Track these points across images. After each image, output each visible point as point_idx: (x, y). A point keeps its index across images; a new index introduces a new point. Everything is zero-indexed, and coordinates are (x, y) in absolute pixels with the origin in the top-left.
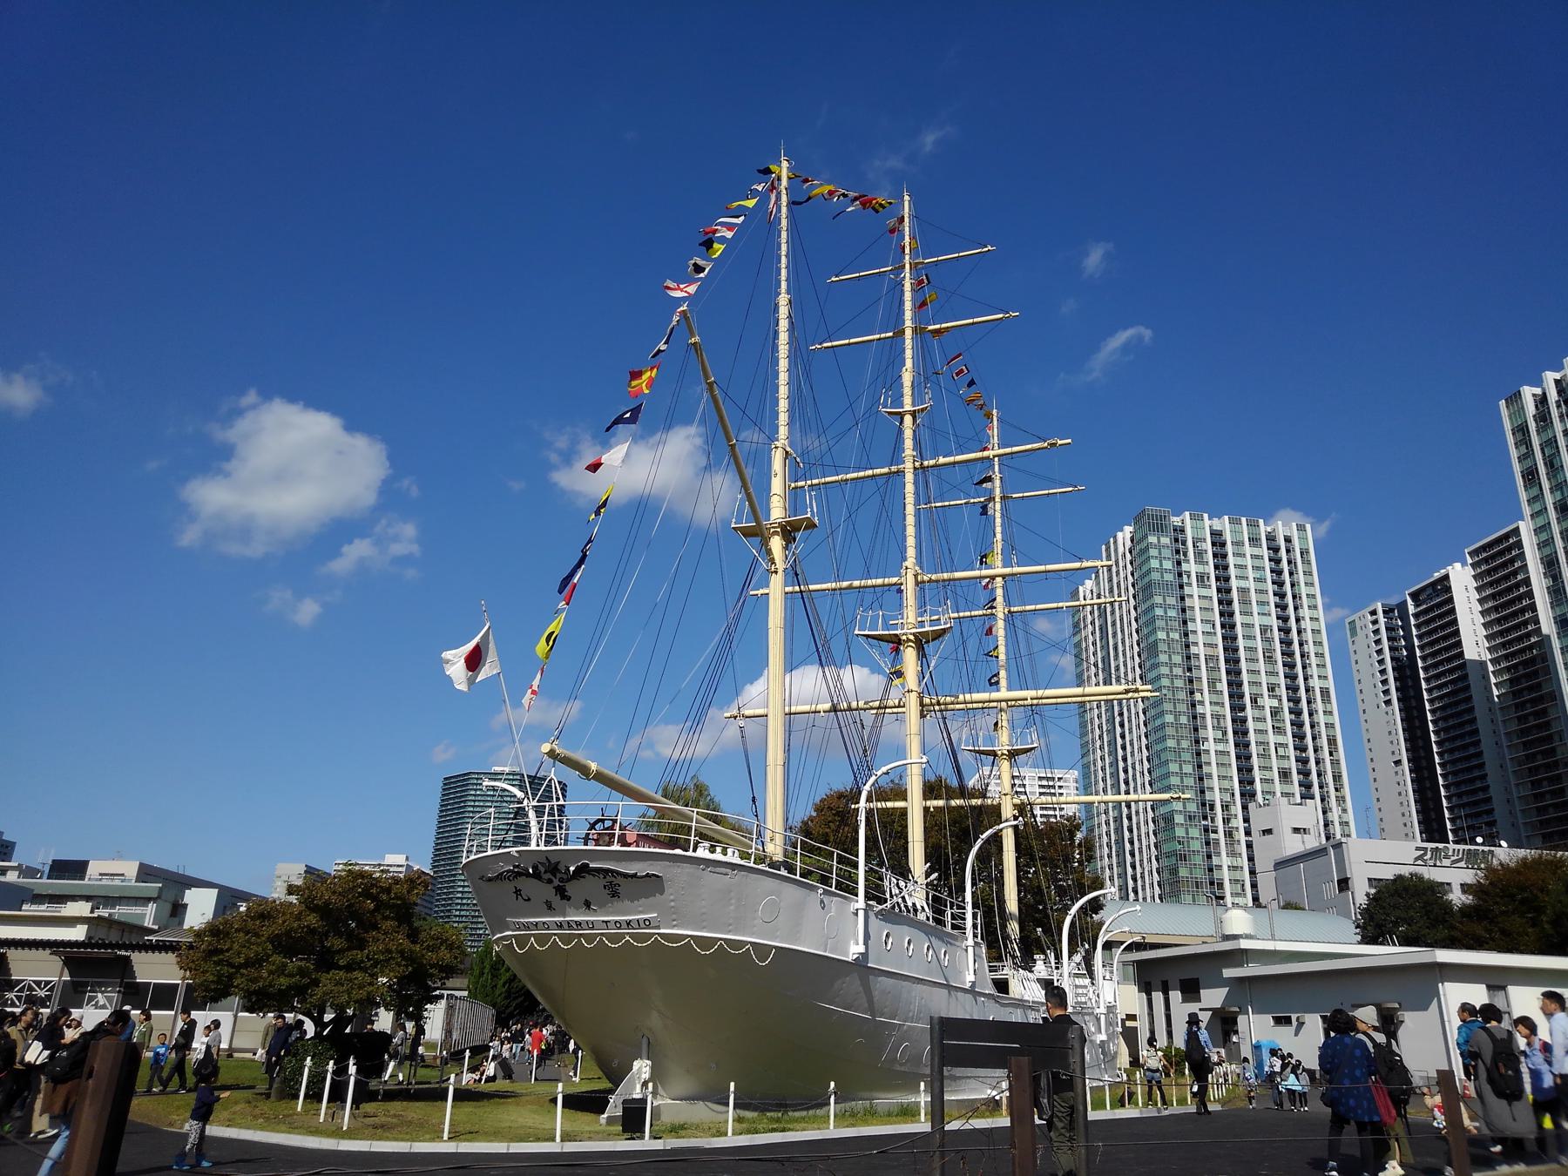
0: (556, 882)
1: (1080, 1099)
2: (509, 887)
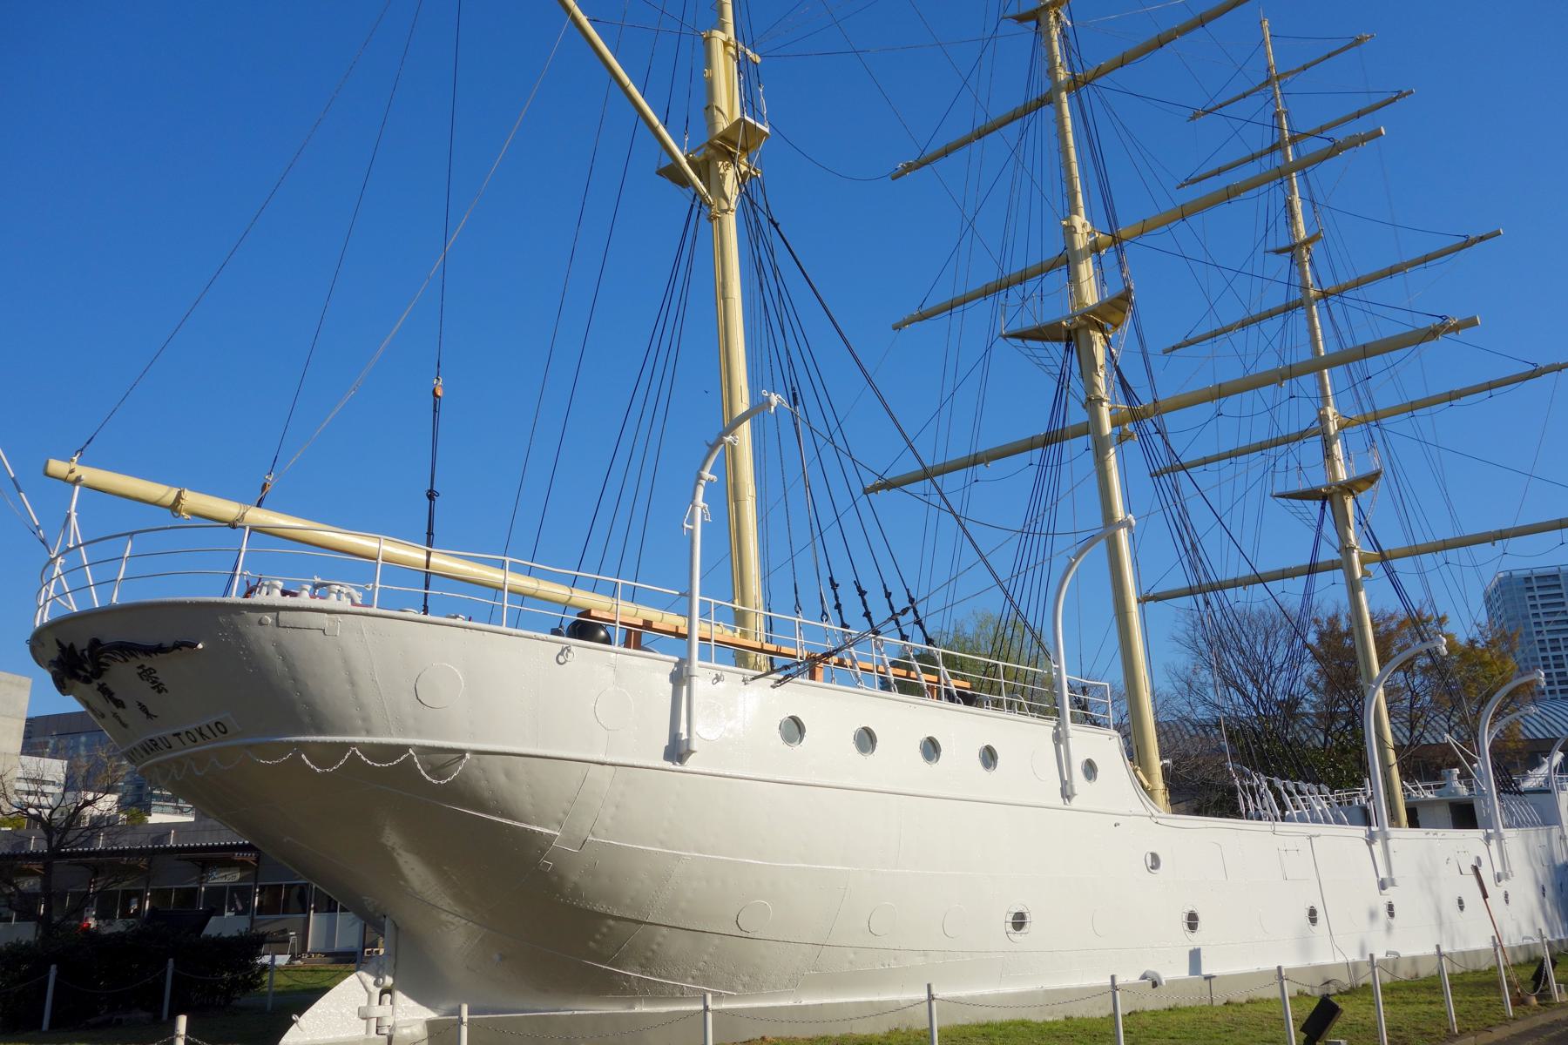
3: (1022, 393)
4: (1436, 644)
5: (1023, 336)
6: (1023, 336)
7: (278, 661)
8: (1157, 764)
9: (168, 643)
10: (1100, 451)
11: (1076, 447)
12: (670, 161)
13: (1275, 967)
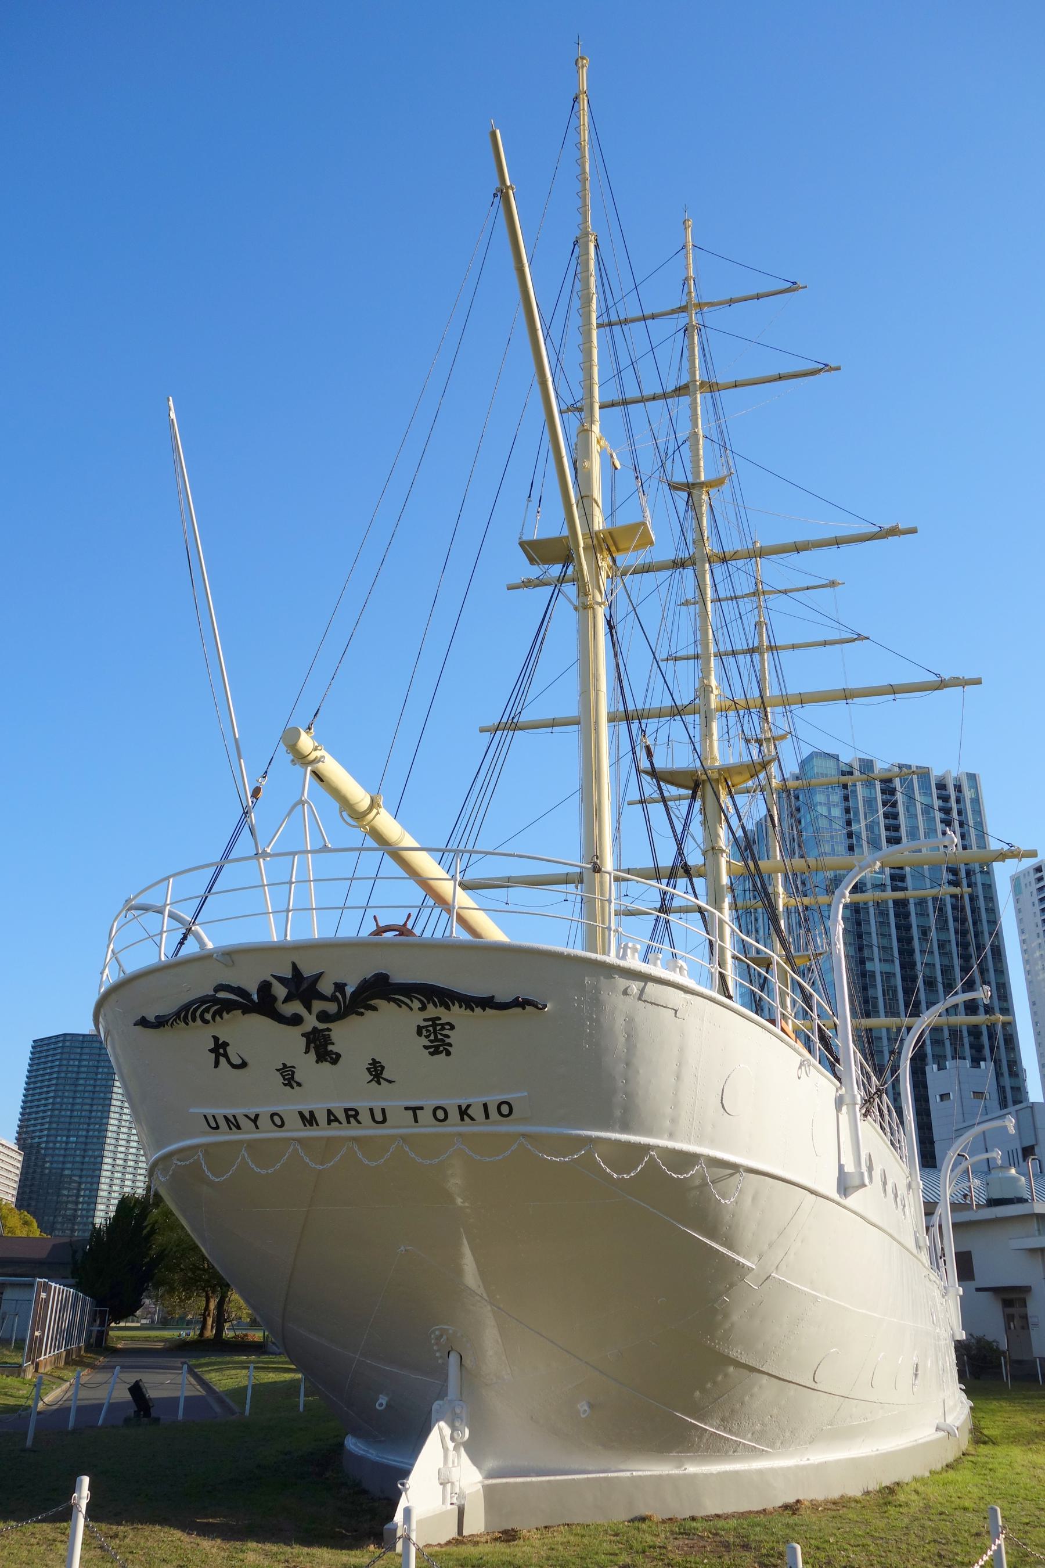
0: (311, 1022)
1: (272, 1358)
2: (198, 1037)
4: (1007, 1123)
7: (622, 1040)
9: (502, 997)
12: (566, 532)
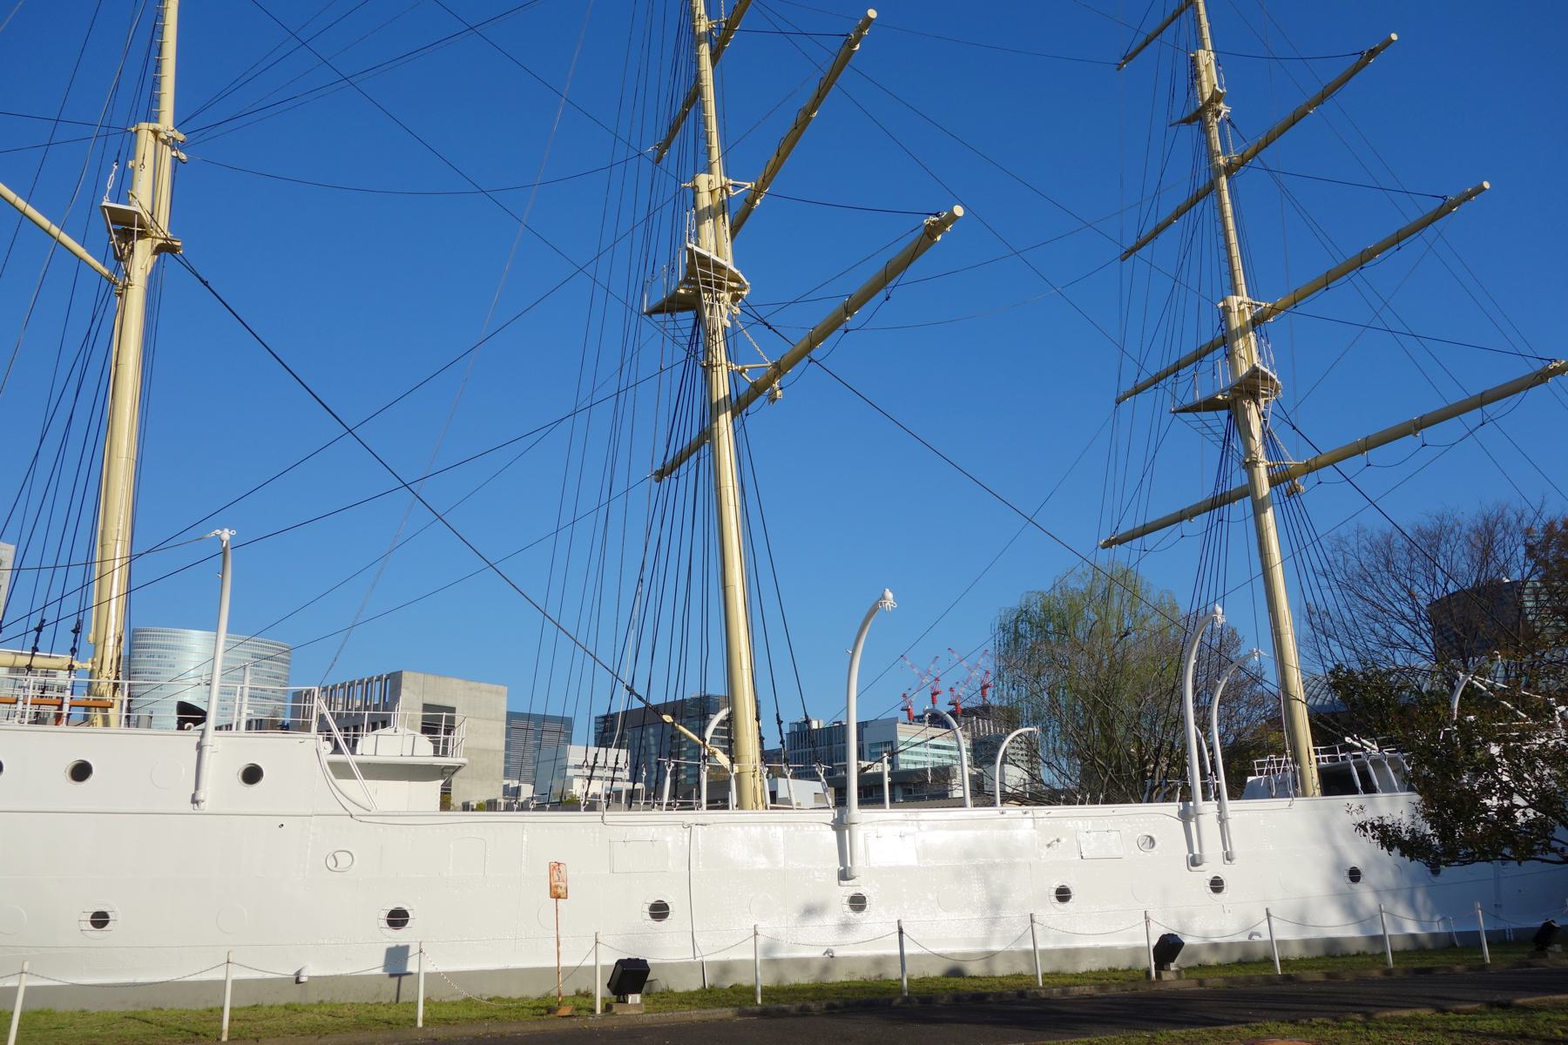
3: (1190, 464)
5: (1195, 408)
6: (1195, 408)
8: (1324, 988)
10: (1259, 508)
11: (1241, 508)
13: (291, 973)
